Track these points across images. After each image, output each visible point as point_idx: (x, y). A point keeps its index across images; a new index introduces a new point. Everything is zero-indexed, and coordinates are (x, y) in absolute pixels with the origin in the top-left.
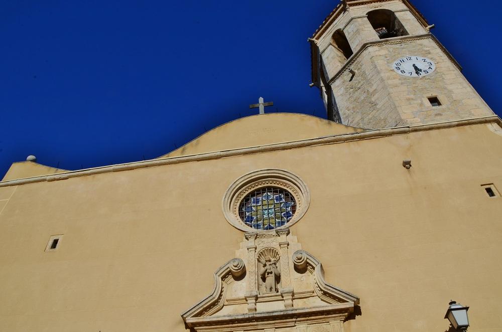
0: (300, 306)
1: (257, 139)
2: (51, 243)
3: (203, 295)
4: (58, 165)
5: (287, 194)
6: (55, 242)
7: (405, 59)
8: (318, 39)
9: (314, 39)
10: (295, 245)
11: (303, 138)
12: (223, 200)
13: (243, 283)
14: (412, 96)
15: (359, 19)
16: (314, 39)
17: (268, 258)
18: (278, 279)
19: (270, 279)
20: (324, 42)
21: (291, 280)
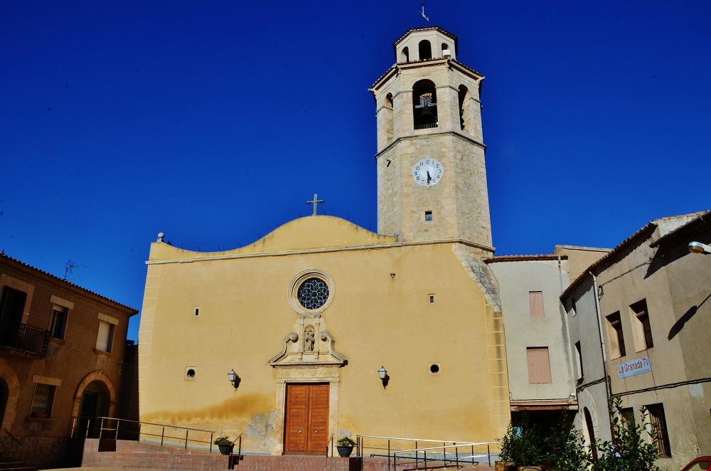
0: (322, 360)
1: (312, 238)
2: (195, 312)
3: (279, 351)
4: (199, 250)
5: (319, 280)
6: (197, 314)
7: (424, 162)
8: (377, 89)
9: (373, 90)
10: (323, 328)
11: (362, 244)
12: (287, 288)
13: (296, 344)
14: (415, 209)
15: (405, 94)
16: (373, 90)
17: (309, 331)
18: (313, 343)
19: (310, 342)
20: (380, 95)
21: (319, 345)
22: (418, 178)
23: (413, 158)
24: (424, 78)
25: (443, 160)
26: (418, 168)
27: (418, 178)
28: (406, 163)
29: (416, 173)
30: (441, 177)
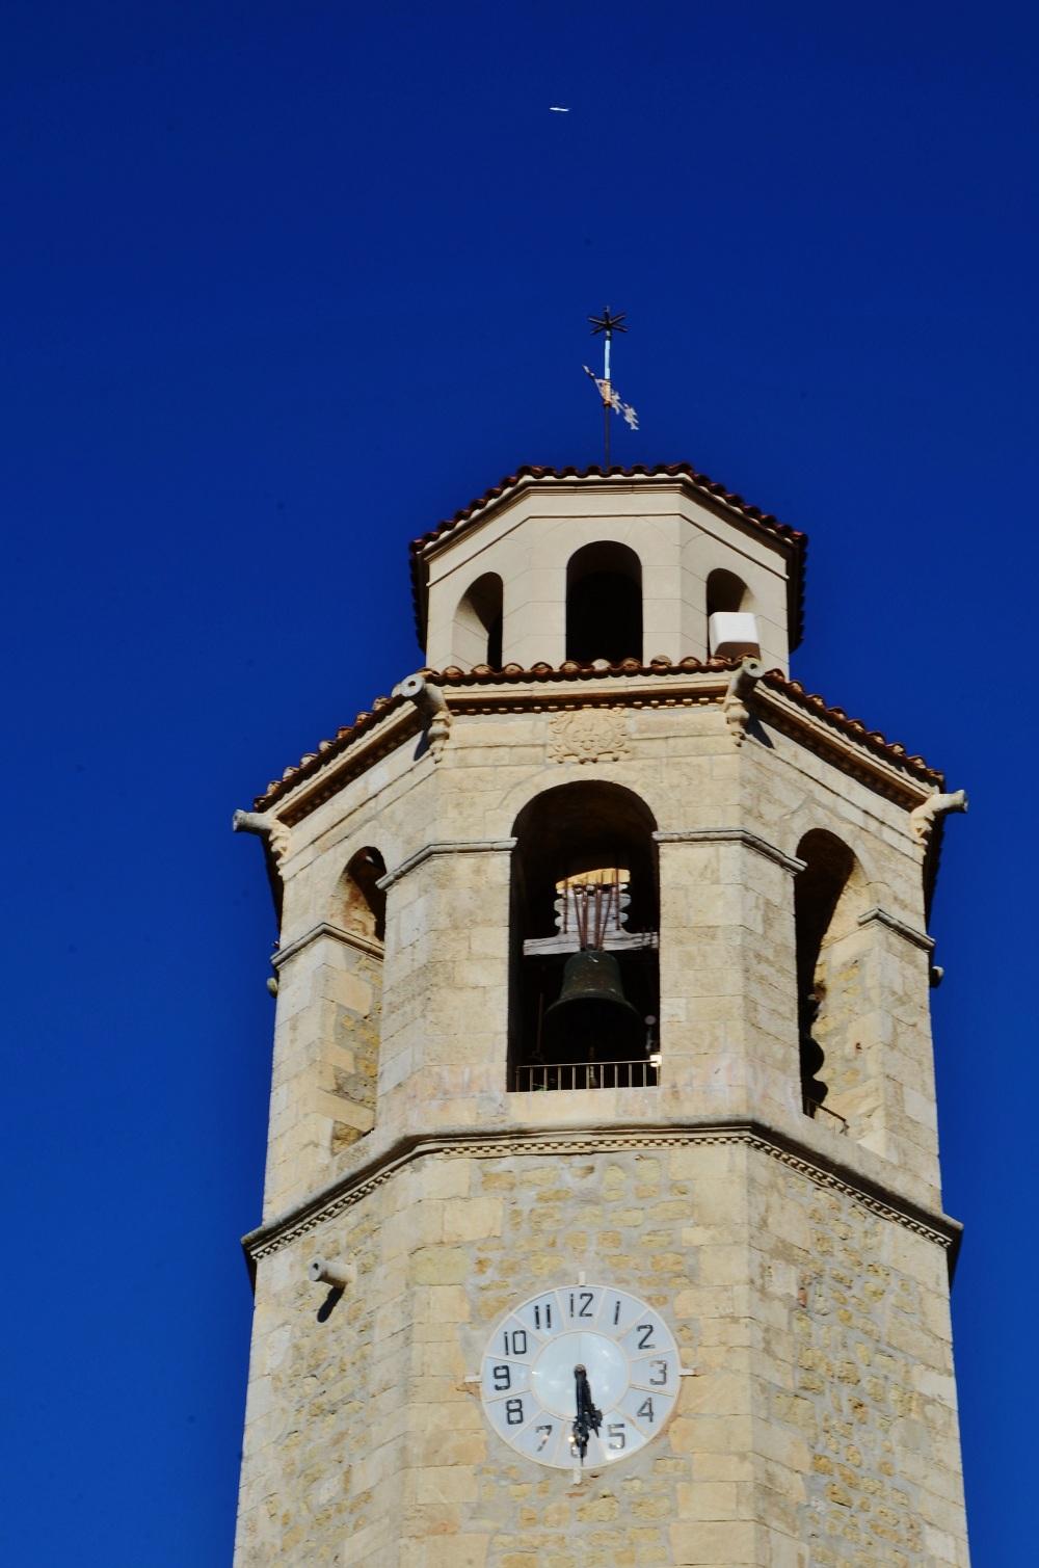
22: (515, 1411)
23: (491, 1274)
24: (590, 773)
25: (685, 1301)
26: (516, 1343)
27: (515, 1411)
28: (444, 1303)
29: (504, 1374)
30: (662, 1411)
